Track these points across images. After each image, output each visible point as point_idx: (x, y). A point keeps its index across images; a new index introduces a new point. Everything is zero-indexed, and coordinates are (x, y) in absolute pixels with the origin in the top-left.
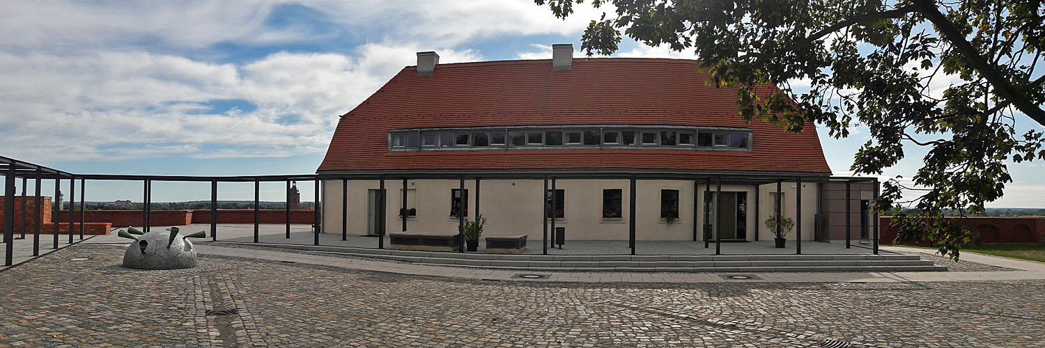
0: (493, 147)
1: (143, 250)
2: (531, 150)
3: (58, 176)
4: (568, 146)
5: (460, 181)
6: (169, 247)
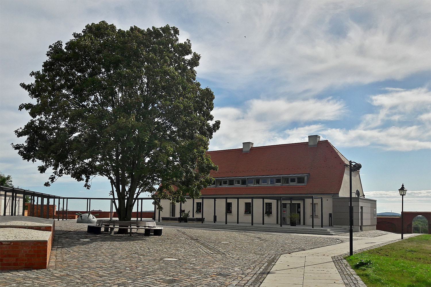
0: (276, 184)
1: (81, 218)
2: (263, 186)
3: (54, 197)
4: (237, 185)
5: (312, 199)
6: (88, 218)
